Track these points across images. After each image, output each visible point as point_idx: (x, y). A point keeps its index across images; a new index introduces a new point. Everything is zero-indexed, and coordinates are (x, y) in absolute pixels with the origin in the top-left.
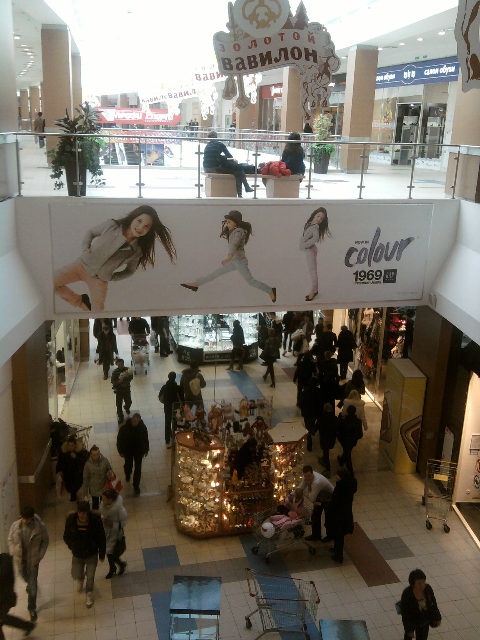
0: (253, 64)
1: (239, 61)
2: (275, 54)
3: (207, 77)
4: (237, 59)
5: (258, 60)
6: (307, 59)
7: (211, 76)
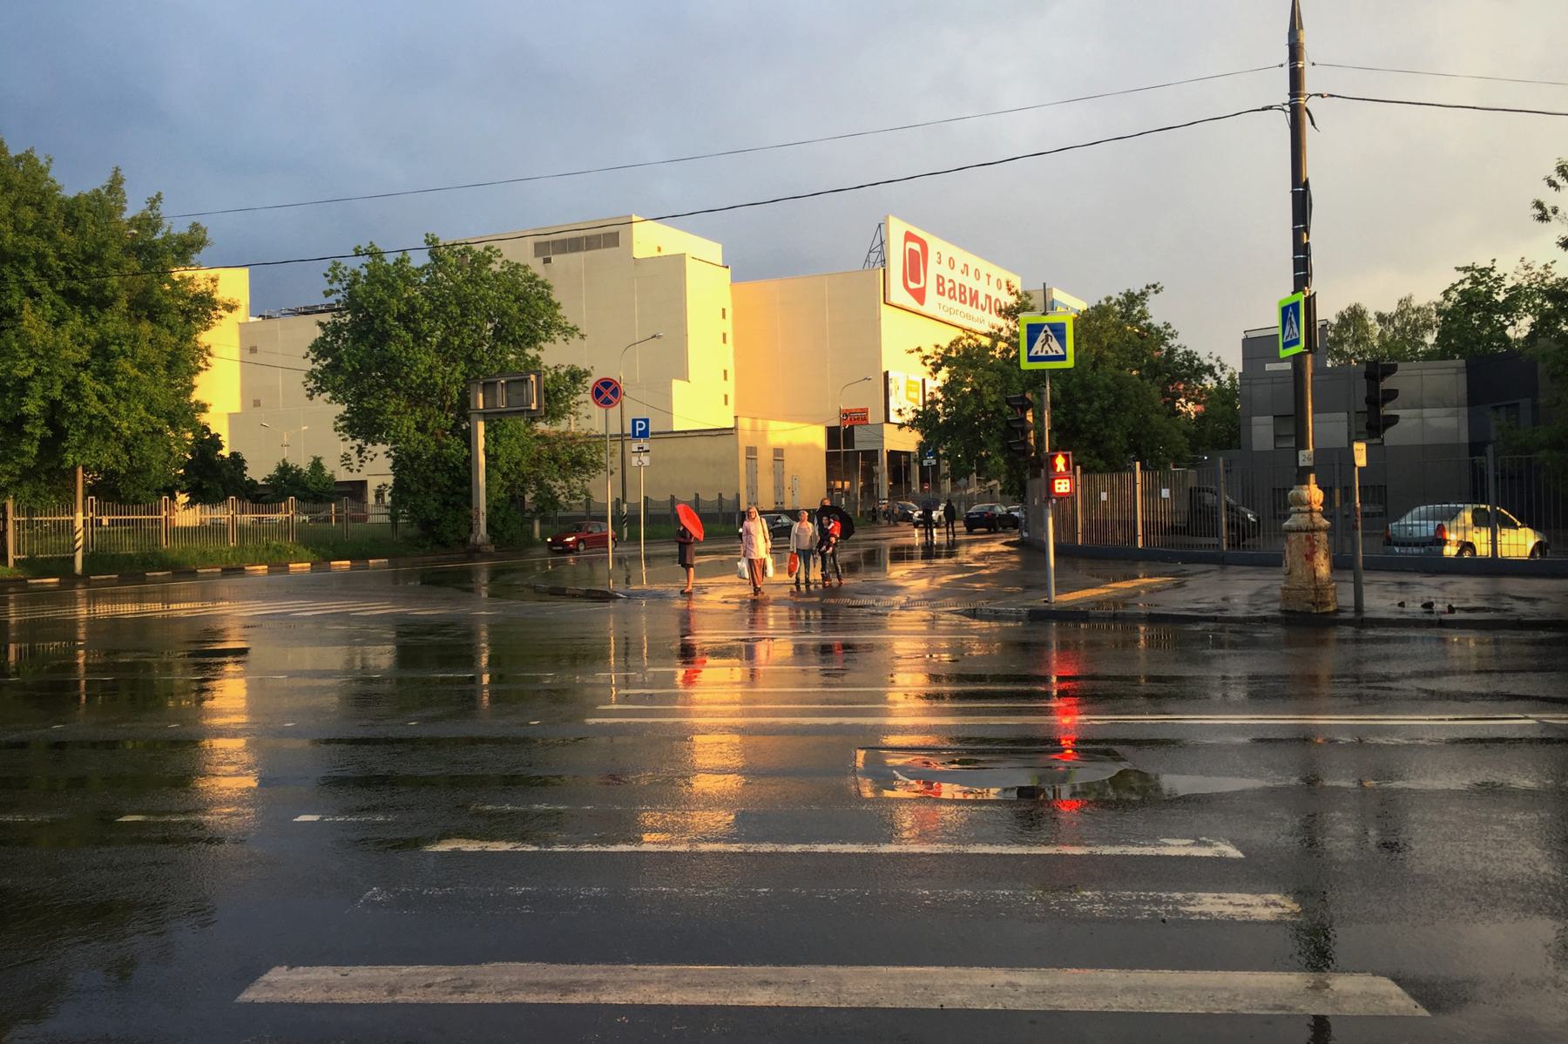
0: (963, 298)
1: (951, 285)
2: (982, 300)
3: (953, 289)
4: (951, 281)
7: (961, 293)
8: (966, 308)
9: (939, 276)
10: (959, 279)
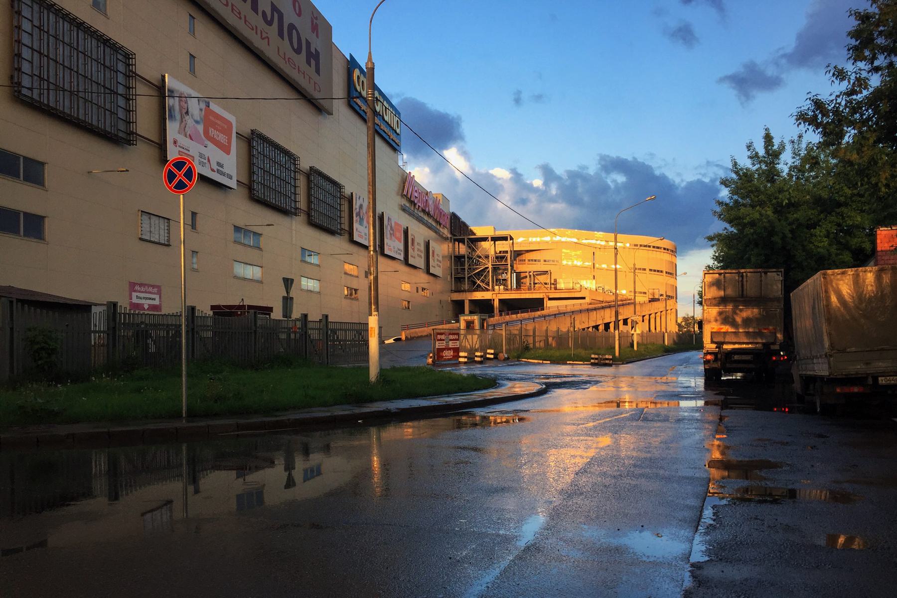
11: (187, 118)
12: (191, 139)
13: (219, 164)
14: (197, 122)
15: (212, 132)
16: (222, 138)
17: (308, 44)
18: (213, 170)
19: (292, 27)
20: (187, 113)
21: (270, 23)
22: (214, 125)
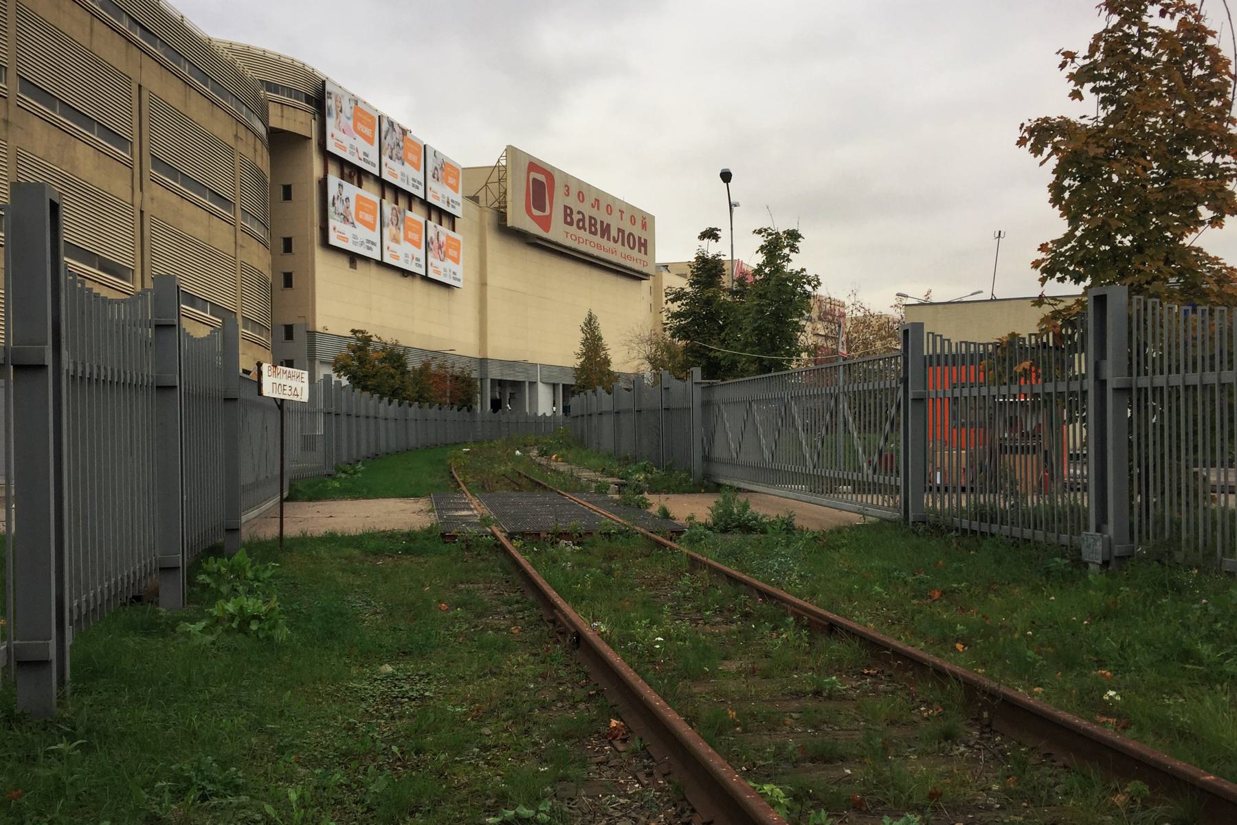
1: (580, 217)
2: (614, 233)
3: (583, 220)
5: (598, 226)
6: (640, 251)
7: (591, 225)
8: (597, 239)
9: (566, 207)
10: (588, 211)
11: (341, 114)
12: (344, 132)
13: (365, 154)
14: (348, 118)
15: (360, 127)
16: (367, 131)
17: (640, 238)
18: (360, 159)
19: (630, 234)
20: (341, 111)
21: (616, 241)
22: (361, 120)
